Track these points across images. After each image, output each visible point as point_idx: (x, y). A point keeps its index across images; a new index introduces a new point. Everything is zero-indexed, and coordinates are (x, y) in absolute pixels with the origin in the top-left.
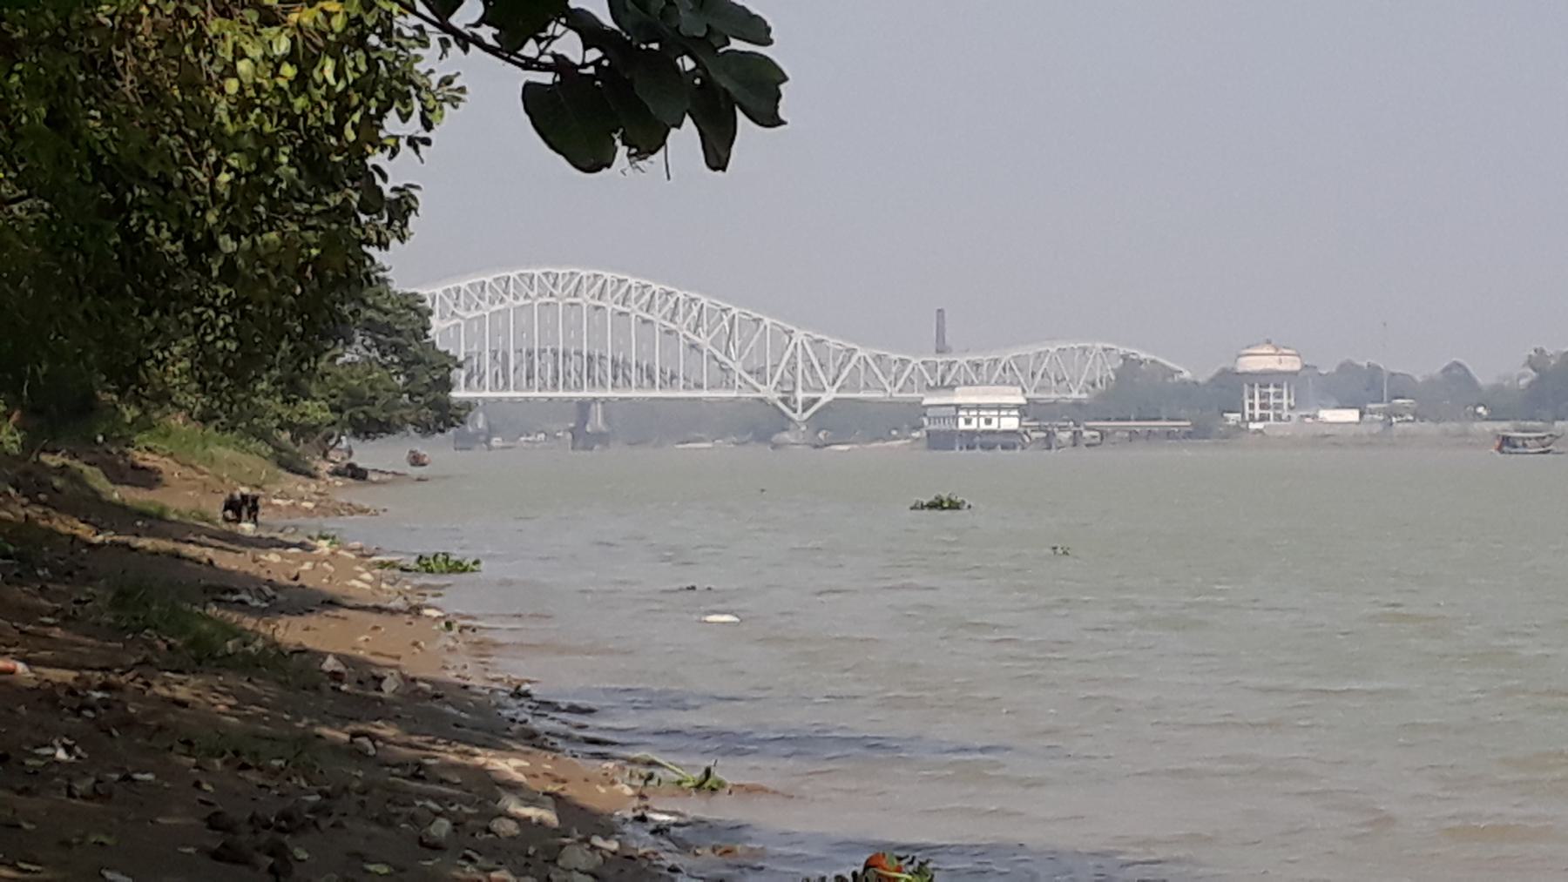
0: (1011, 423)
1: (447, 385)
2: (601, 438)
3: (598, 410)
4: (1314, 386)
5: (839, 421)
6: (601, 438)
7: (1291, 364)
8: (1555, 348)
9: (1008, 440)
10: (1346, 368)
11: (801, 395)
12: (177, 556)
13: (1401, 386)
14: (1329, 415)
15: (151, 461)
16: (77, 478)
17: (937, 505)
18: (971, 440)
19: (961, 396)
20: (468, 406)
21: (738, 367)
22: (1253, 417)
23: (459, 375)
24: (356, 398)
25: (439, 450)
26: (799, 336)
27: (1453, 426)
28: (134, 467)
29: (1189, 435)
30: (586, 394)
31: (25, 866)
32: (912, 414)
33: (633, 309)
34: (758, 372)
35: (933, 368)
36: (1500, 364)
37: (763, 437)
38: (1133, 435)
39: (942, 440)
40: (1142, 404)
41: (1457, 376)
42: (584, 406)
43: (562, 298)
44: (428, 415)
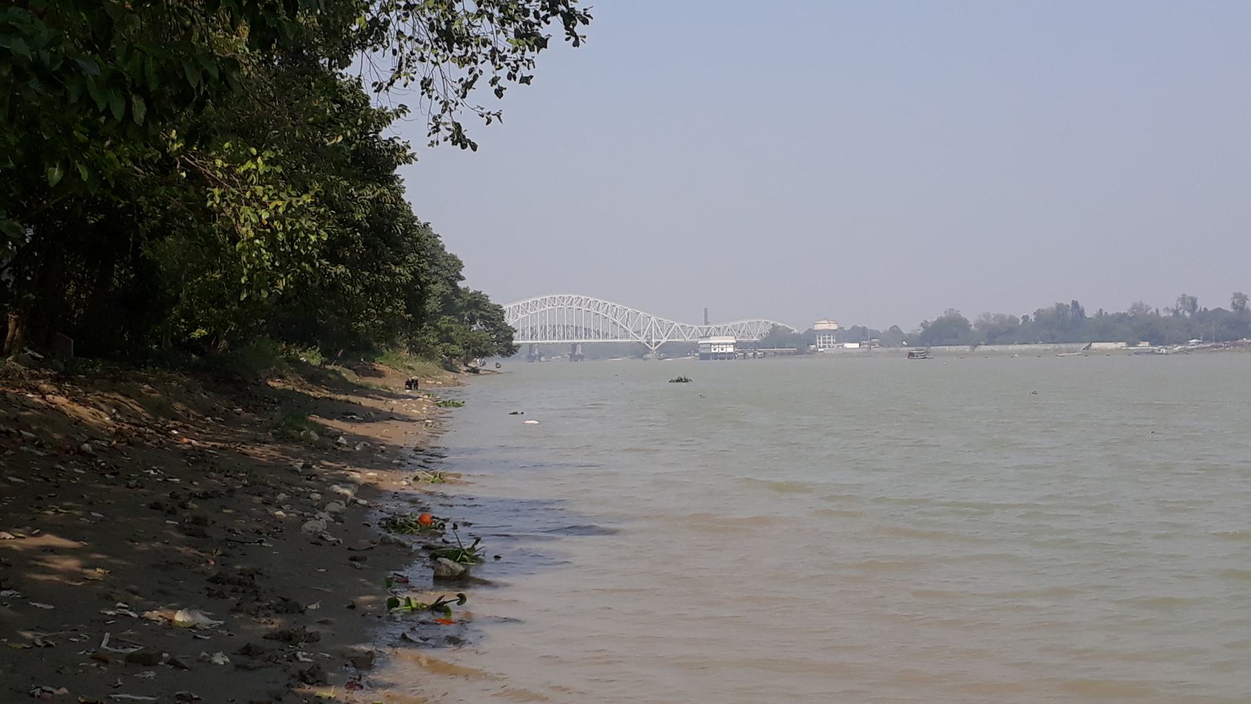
0: (730, 350)
2: (581, 357)
5: (669, 350)
6: (581, 357)
7: (834, 327)
9: (730, 356)
13: (875, 334)
14: (848, 345)
15: (381, 368)
17: (679, 380)
18: (716, 356)
19: (713, 340)
20: (519, 346)
21: (631, 330)
22: (821, 346)
23: (515, 335)
24: (475, 344)
25: (507, 364)
26: (653, 319)
29: (796, 353)
31: (327, 463)
32: (694, 347)
33: (592, 309)
34: (638, 332)
36: (911, 326)
39: (705, 357)
40: (785, 343)
41: (895, 331)
42: (574, 345)
43: (565, 305)
44: (505, 350)
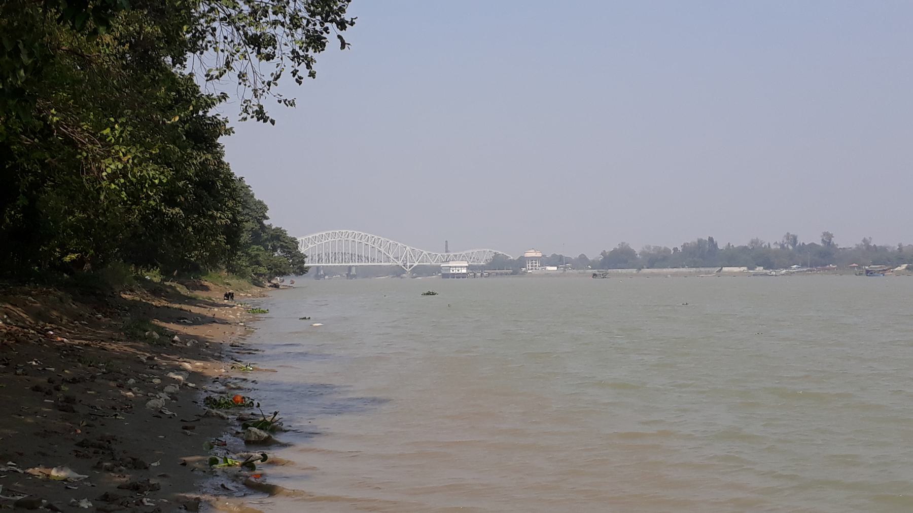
0: (464, 271)
1: (304, 263)
3: (354, 269)
4: (545, 261)
5: (419, 271)
6: (355, 276)
7: (539, 255)
8: (905, 244)
9: (463, 276)
10: (554, 255)
11: (408, 264)
12: (181, 309)
13: (568, 260)
14: (549, 268)
15: (206, 283)
16: (174, 288)
18: (453, 276)
20: (308, 267)
21: (391, 257)
22: (529, 269)
23: (306, 260)
24: (276, 266)
25: (299, 281)
26: (408, 248)
27: (581, 271)
28: (202, 285)
29: (512, 274)
30: (351, 264)
32: (438, 269)
34: (397, 258)
35: (443, 256)
36: (594, 255)
37: (398, 276)
38: (497, 274)
39: (445, 276)
40: (504, 266)
41: (583, 258)
42: (350, 267)
